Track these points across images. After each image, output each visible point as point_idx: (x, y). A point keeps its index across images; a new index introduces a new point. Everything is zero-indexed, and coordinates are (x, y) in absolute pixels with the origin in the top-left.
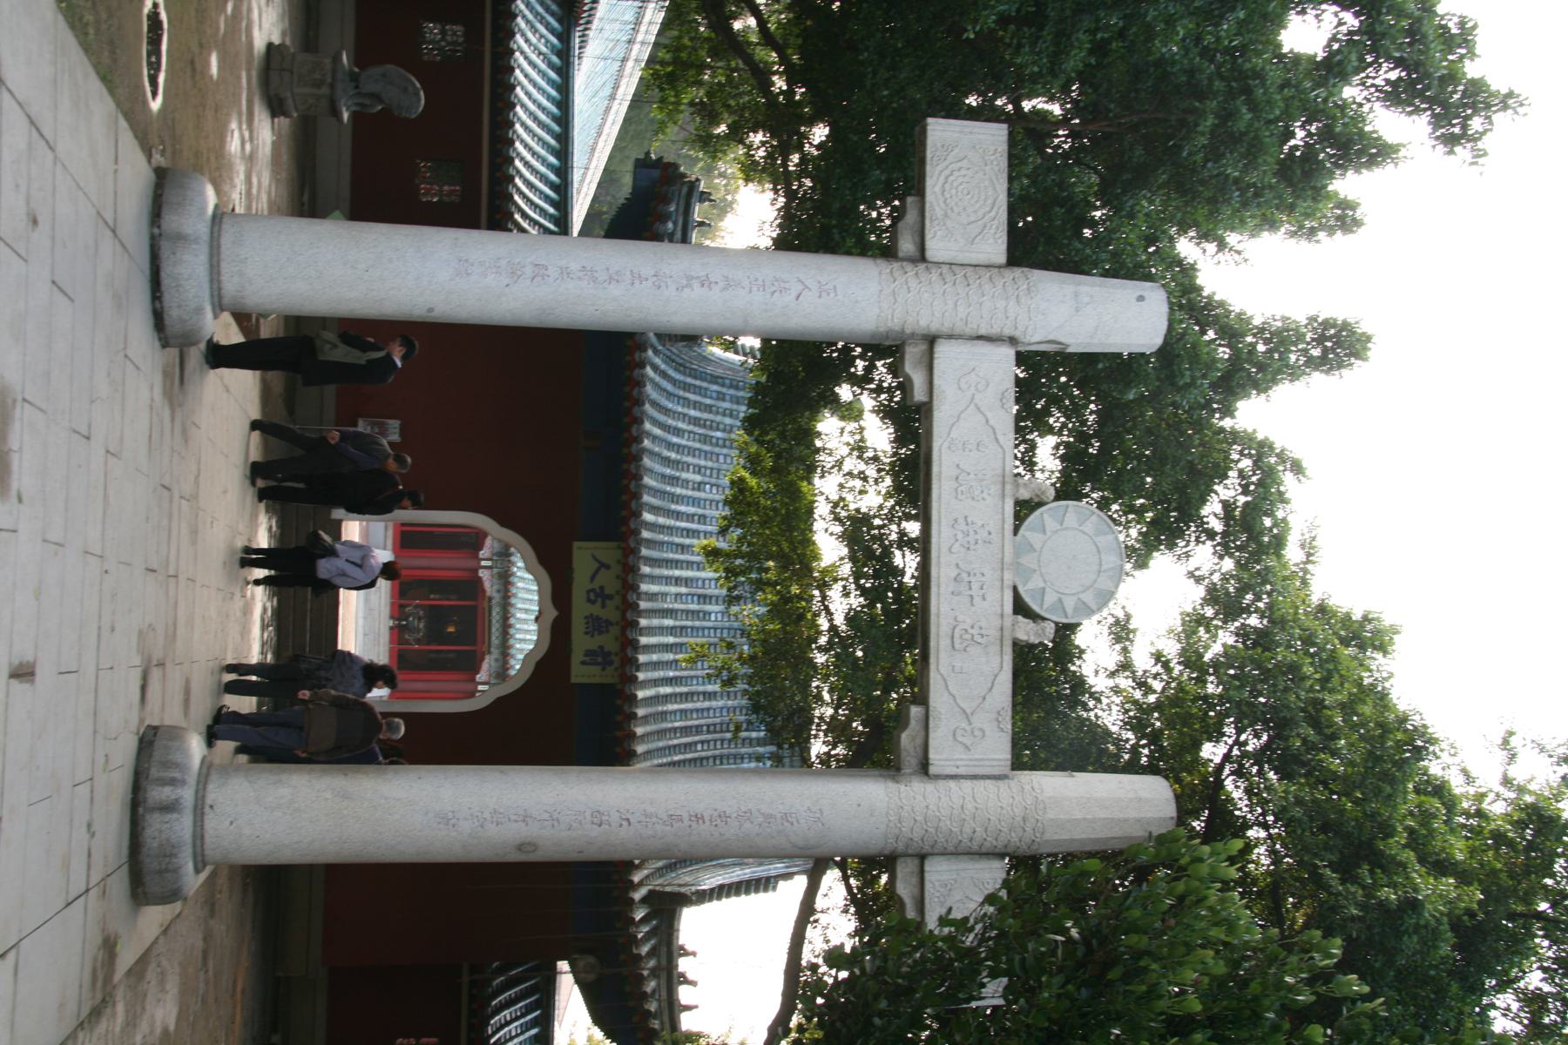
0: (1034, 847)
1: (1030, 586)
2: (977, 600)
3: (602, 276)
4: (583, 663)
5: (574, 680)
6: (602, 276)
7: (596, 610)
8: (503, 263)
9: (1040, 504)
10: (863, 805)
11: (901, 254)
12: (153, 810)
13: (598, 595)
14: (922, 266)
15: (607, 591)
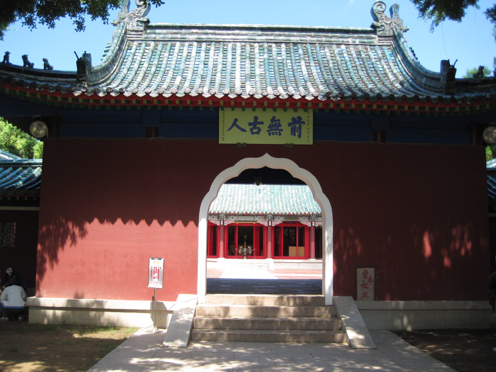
4: (300, 136)
5: (311, 143)
7: (264, 128)
13: (255, 125)
15: (252, 121)
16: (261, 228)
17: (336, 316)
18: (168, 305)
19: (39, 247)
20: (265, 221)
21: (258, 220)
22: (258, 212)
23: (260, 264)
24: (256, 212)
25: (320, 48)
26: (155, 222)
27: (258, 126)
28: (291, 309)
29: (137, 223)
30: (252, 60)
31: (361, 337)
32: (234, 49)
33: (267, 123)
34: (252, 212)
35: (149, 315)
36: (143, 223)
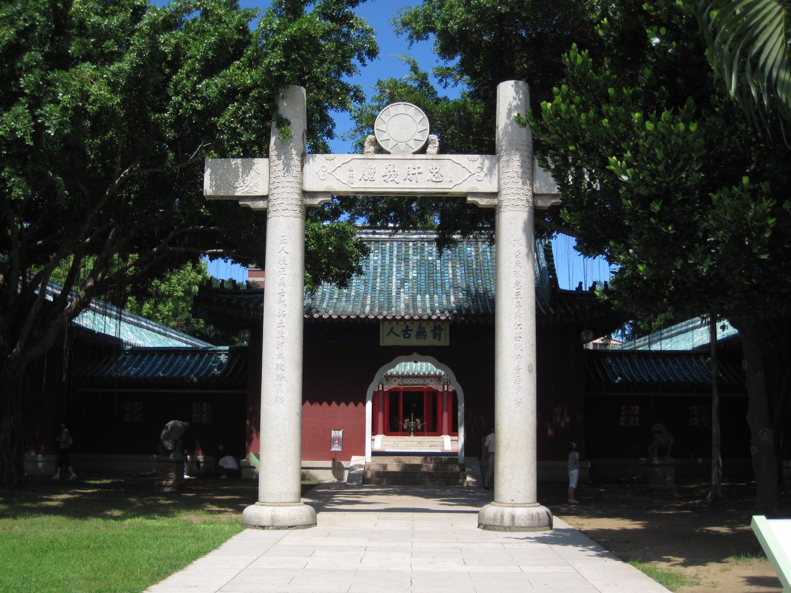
0: (529, 144)
1: (413, 146)
2: (420, 171)
3: (281, 340)
4: (439, 339)
5: (448, 344)
6: (281, 340)
7: (413, 334)
8: (276, 383)
9: (376, 140)
10: (513, 223)
11: (265, 207)
12: (513, 523)
14: (271, 197)
16: (434, 393)
17: (463, 470)
18: (345, 464)
19: (248, 422)
20: (439, 384)
21: (430, 383)
22: (429, 373)
23: (432, 443)
24: (427, 373)
25: (467, 245)
26: (334, 404)
27: (409, 332)
28: (431, 466)
29: (321, 404)
30: (406, 260)
31: (474, 480)
32: (391, 248)
33: (416, 330)
34: (421, 374)
35: (330, 471)
36: (325, 404)
